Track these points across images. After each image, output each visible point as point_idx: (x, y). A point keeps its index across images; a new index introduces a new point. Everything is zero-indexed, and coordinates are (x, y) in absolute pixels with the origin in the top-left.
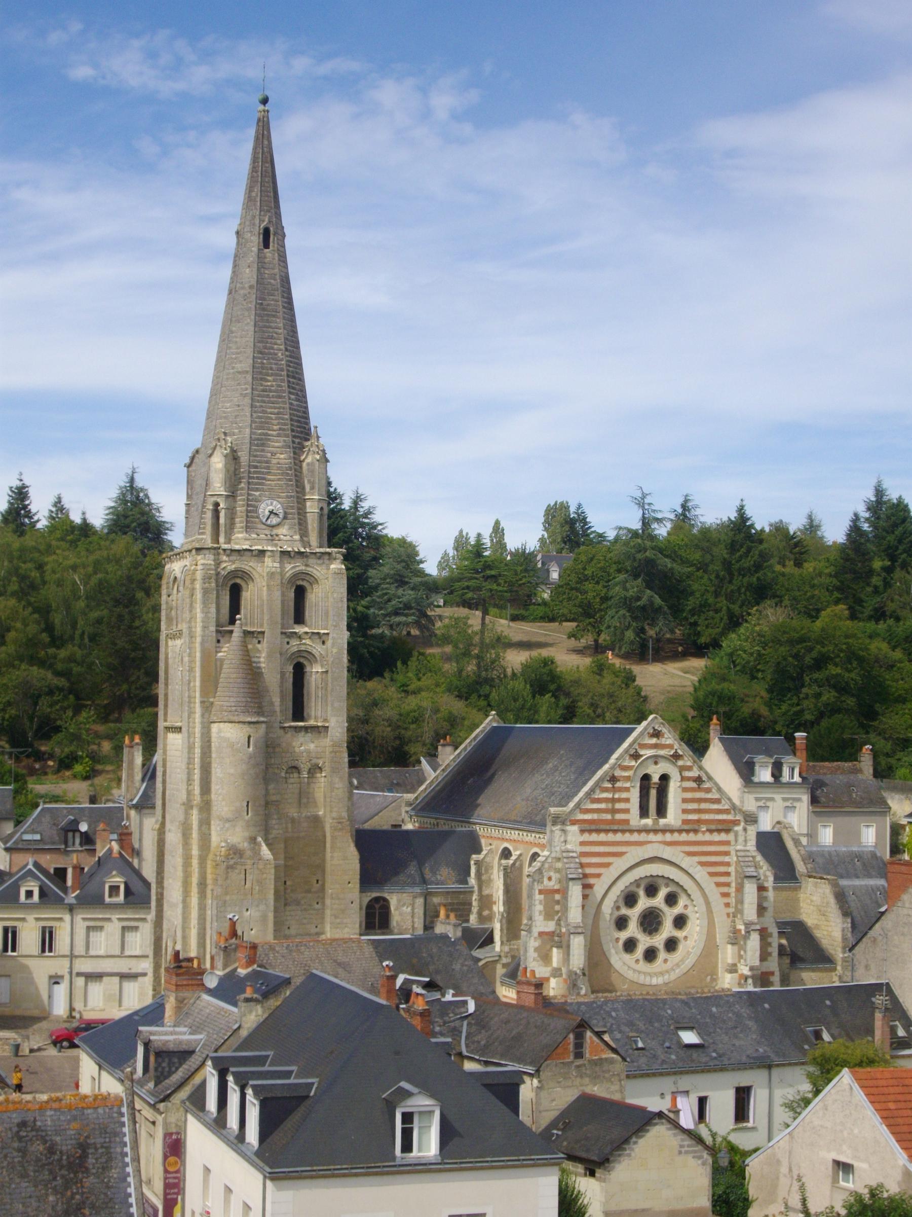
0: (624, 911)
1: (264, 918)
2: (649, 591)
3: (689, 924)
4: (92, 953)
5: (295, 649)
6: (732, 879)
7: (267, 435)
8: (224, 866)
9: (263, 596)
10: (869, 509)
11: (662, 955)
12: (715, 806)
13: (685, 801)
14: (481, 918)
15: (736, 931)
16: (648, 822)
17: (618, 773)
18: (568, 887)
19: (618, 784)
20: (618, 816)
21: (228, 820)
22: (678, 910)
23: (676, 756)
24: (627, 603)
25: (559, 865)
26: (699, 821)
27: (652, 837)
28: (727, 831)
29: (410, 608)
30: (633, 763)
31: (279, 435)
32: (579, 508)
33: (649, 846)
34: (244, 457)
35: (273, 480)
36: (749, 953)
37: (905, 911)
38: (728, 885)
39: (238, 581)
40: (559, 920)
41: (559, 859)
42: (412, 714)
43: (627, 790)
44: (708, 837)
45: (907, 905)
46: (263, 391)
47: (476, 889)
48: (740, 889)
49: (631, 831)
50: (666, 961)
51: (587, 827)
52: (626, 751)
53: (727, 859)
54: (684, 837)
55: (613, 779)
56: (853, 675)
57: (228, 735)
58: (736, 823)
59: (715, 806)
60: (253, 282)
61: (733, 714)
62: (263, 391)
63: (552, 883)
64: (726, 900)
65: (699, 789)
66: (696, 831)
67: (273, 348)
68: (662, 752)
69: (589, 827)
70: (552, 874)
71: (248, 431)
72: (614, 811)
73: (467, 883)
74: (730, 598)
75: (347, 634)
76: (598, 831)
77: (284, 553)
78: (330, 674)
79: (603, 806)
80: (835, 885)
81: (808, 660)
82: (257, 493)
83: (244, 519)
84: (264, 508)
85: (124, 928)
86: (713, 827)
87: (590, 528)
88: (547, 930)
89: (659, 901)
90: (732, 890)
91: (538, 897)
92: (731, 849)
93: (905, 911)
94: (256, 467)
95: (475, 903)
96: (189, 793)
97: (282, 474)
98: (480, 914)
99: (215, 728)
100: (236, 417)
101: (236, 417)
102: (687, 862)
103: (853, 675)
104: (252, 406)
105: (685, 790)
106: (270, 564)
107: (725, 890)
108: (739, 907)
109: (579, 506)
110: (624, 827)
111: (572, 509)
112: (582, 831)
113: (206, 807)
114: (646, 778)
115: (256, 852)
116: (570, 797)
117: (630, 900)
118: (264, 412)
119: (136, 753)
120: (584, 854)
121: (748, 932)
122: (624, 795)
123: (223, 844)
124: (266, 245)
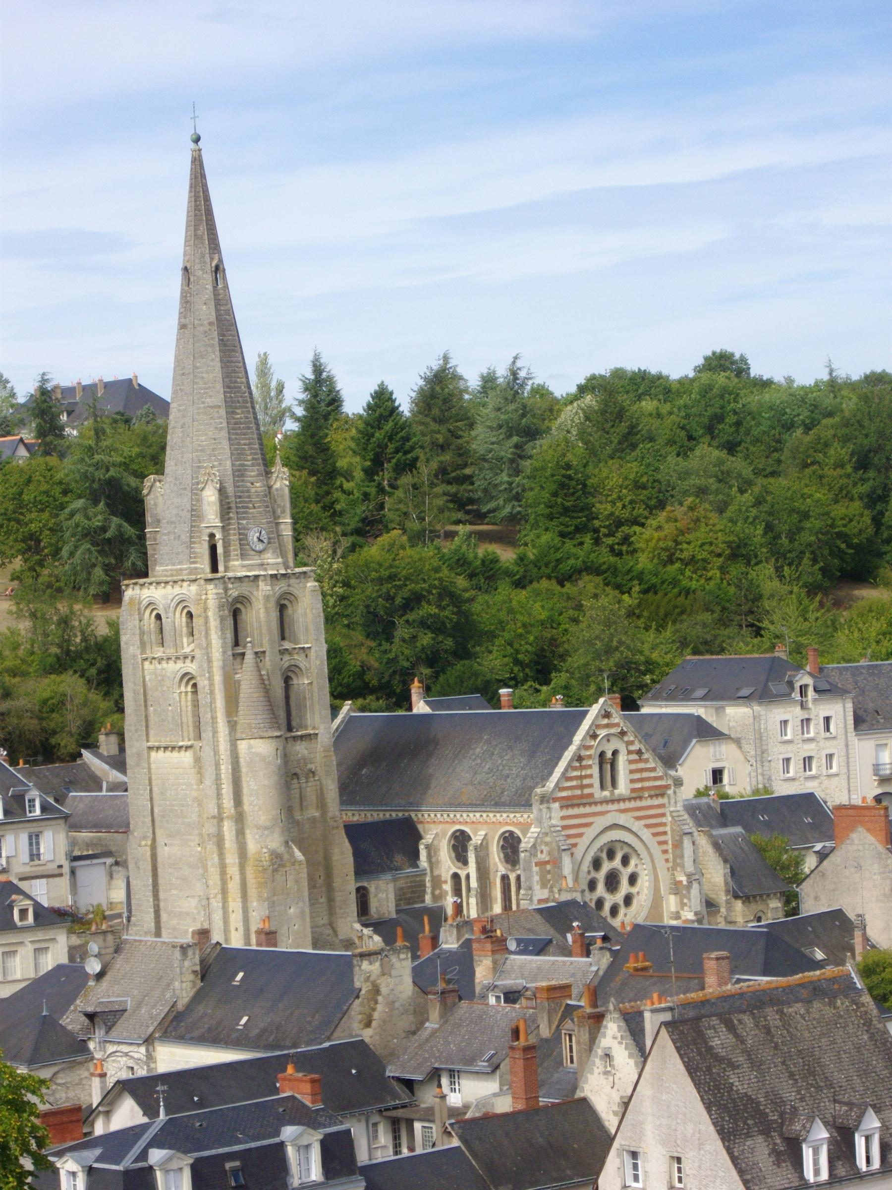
0: (593, 874)
1: (303, 912)
2: (115, 518)
3: (639, 881)
4: (10, 978)
5: (287, 665)
6: (668, 837)
8: (270, 871)
9: (259, 616)
10: (306, 389)
11: (622, 910)
12: (652, 774)
13: (631, 772)
14: (435, 898)
15: (678, 883)
16: (606, 793)
17: (584, 753)
18: (561, 858)
19: (584, 763)
20: (587, 791)
21: (266, 828)
22: (631, 869)
23: (623, 733)
24: (93, 535)
25: (548, 839)
26: (642, 789)
27: (611, 807)
28: (662, 795)
30: (592, 743)
31: (253, 465)
33: (609, 815)
34: (230, 490)
36: (693, 900)
37: (855, 847)
38: (665, 842)
39: (239, 606)
40: (551, 887)
41: (546, 834)
42: (50, 702)
43: (590, 767)
44: (649, 802)
45: (856, 842)
47: (428, 871)
48: (678, 845)
49: (596, 803)
50: (625, 915)
51: (565, 803)
52: (587, 732)
53: (664, 820)
54: (633, 804)
55: (580, 758)
56: (447, 613)
57: (259, 750)
58: (667, 787)
59: (652, 774)
60: (213, 318)
61: (342, 668)
63: (544, 856)
64: (665, 856)
65: (640, 760)
66: (641, 798)
67: (236, 382)
69: (568, 803)
70: (543, 847)
71: (229, 463)
72: (582, 787)
73: (417, 866)
76: (573, 806)
79: (574, 783)
80: (711, 836)
81: (398, 601)
82: (244, 522)
84: (253, 536)
85: (36, 950)
86: (652, 793)
88: (543, 897)
89: (617, 862)
90: (669, 847)
91: (535, 869)
92: (666, 810)
93: (855, 847)
94: (240, 497)
95: (428, 884)
96: (220, 807)
98: (433, 893)
99: (242, 746)
100: (213, 450)
101: (213, 450)
102: (637, 826)
103: (447, 613)
104: (230, 439)
105: (631, 762)
106: (264, 588)
107: (664, 847)
108: (678, 861)
110: (587, 800)
112: (562, 807)
113: (240, 818)
114: (602, 755)
115: (292, 855)
117: (597, 864)
118: (239, 444)
120: (565, 828)
121: (690, 883)
122: (589, 772)
123: (265, 850)
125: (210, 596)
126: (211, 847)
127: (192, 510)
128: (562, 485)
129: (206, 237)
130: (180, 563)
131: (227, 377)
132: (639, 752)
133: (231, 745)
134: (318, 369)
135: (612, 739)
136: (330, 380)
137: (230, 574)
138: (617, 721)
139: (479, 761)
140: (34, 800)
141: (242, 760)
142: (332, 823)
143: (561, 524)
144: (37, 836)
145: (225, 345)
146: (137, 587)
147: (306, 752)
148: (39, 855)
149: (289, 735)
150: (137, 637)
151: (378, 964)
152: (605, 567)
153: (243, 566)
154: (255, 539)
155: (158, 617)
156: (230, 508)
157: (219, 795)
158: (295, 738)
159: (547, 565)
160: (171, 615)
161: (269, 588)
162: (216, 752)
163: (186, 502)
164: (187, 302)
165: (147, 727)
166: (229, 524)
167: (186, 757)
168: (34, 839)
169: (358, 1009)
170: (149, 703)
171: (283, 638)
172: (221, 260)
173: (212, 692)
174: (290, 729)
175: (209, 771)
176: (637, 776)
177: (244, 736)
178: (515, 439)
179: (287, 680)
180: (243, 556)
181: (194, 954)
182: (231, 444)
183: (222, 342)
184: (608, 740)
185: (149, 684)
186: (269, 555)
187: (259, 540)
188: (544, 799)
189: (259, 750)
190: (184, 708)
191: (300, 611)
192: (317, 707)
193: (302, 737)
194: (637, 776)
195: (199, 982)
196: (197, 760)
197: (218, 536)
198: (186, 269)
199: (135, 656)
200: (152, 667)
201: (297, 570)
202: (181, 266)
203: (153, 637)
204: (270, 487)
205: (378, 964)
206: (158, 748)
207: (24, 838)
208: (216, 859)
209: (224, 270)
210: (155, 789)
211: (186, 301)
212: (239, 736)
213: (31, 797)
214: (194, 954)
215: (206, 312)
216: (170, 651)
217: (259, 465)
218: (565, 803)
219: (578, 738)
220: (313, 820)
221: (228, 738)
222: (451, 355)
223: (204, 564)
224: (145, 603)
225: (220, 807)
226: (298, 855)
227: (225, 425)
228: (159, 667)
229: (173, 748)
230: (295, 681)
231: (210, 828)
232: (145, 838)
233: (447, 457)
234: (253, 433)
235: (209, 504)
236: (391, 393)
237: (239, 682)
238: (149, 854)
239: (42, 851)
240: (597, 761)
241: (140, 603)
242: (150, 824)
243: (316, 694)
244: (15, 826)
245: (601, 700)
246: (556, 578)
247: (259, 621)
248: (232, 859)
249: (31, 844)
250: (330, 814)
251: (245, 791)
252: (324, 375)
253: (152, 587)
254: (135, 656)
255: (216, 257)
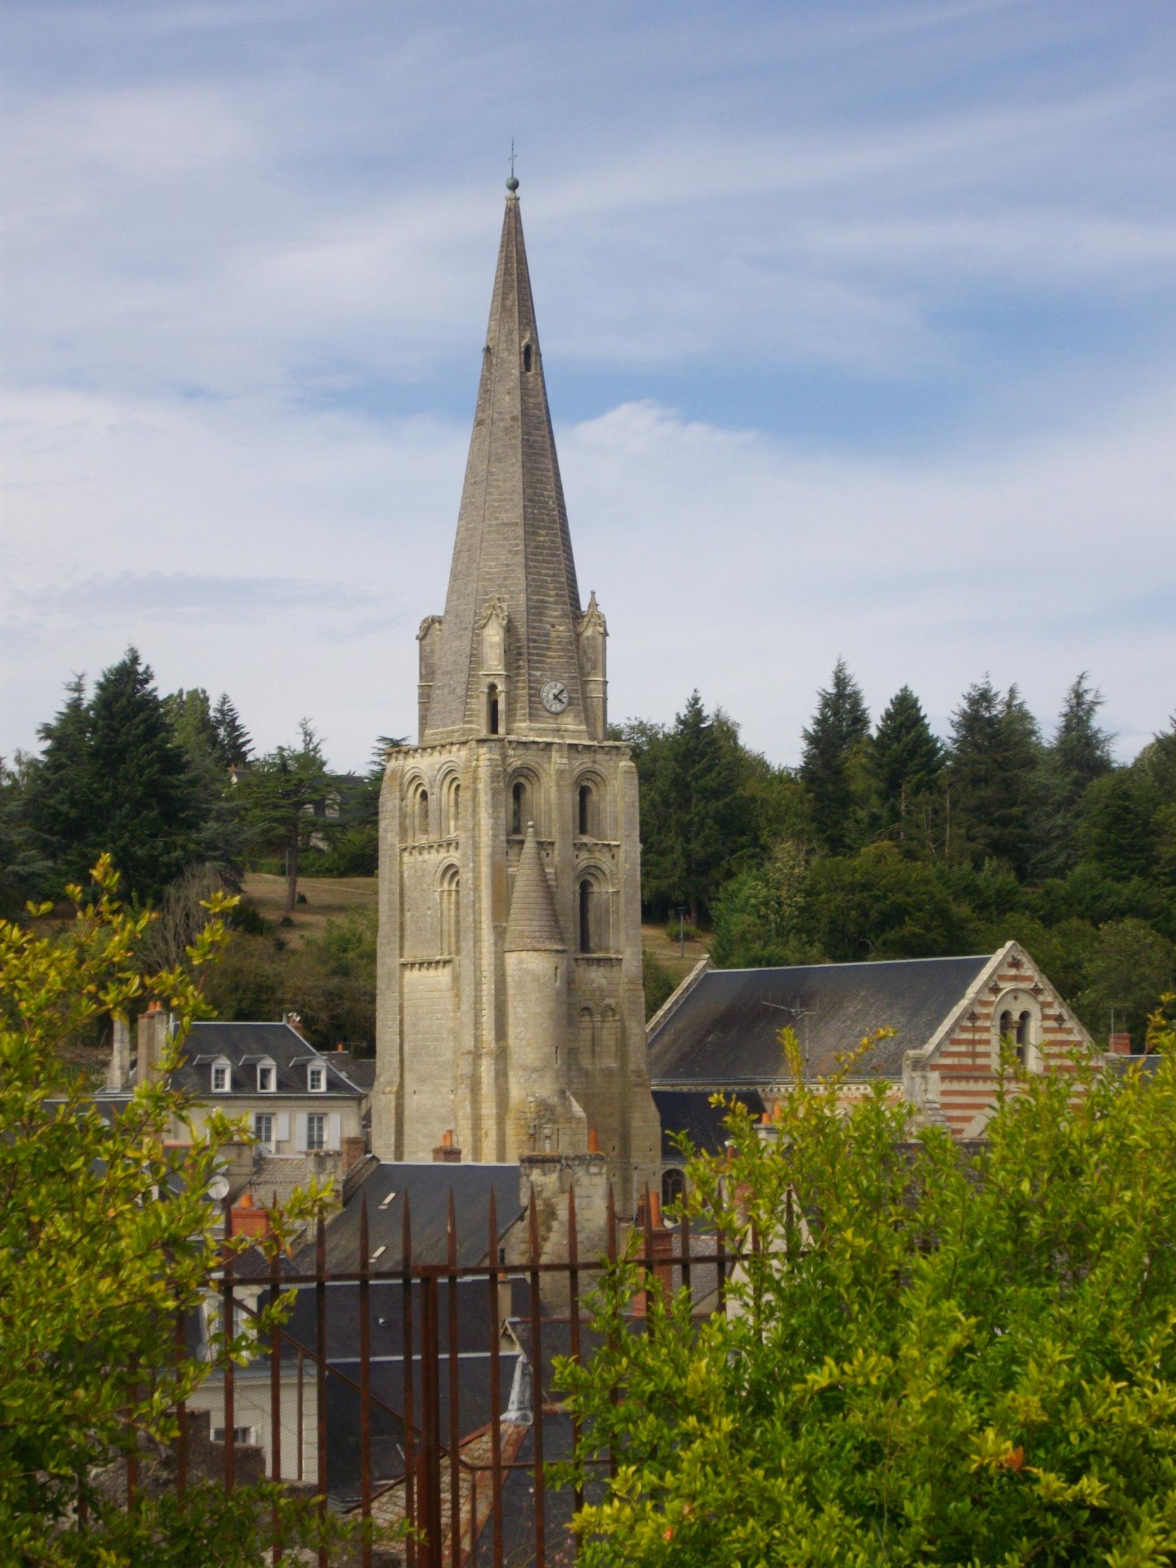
5: (584, 864)
7: (542, 601)
9: (550, 796)
17: (979, 1010)
19: (979, 1023)
20: (980, 1061)
21: (535, 1070)
23: (1036, 991)
29: (216, 848)
30: (992, 998)
31: (556, 603)
32: (224, 703)
34: (522, 630)
35: (554, 658)
39: (522, 780)
43: (987, 1029)
46: (537, 547)
52: (986, 983)
55: (973, 1017)
57: (533, 966)
60: (517, 411)
62: (537, 547)
65: (1060, 1030)
68: (1022, 985)
69: (951, 1074)
71: (523, 597)
72: (974, 1055)
74: (684, 831)
75: (639, 847)
76: (959, 1078)
77: (571, 747)
78: (622, 895)
79: (963, 1048)
81: (874, 915)
83: (526, 705)
84: (549, 691)
87: (241, 735)
96: (477, 1038)
97: (563, 650)
99: (511, 959)
100: (505, 579)
101: (505, 579)
103: (933, 935)
104: (526, 566)
105: (1046, 1030)
106: (558, 759)
109: (225, 700)
111: (214, 703)
112: (943, 1079)
113: (502, 1055)
114: (1005, 1016)
115: (568, 1109)
116: (924, 1042)
119: (158, 1026)
120: (945, 1106)
122: (985, 1036)
123: (531, 1099)
124: (528, 369)
125: (482, 763)
126: (464, 1091)
127: (472, 655)
128: (1117, 819)
129: (516, 309)
130: (453, 723)
131: (530, 487)
132: (1059, 1018)
133: (497, 958)
134: (841, 681)
135: (1023, 997)
136: (855, 698)
137: (512, 737)
138: (1029, 973)
139: (849, 1022)
140: (319, 1073)
141: (509, 980)
142: (633, 1078)
143: (1113, 866)
144: (321, 1120)
145: (531, 447)
146: (401, 756)
147: (604, 982)
148: (320, 1143)
149: (580, 956)
150: (397, 821)
151: (554, 1176)
152: (1155, 910)
153: (531, 729)
154: (551, 697)
155: (424, 795)
156: (520, 654)
157: (477, 1024)
158: (589, 961)
159: (1080, 902)
160: (436, 790)
161: (565, 761)
162: (477, 967)
163: (465, 644)
164: (487, 391)
165: (402, 938)
166: (518, 675)
167: (443, 976)
168: (316, 1122)
169: (521, 1235)
170: (406, 907)
171: (583, 830)
172: (535, 339)
173: (476, 889)
174: (584, 946)
175: (468, 991)
176: (1055, 1050)
177: (513, 947)
178: (1075, 773)
179: (585, 887)
180: (532, 716)
181: (335, 1167)
182: (528, 573)
183: (527, 444)
184: (1016, 998)
185: (407, 882)
186: (569, 720)
187: (556, 697)
188: (918, 1064)
189: (532, 967)
190: (445, 912)
191: (609, 798)
192: (623, 926)
193: (599, 961)
194: (1055, 1050)
195: (340, 1205)
196: (456, 978)
197: (500, 687)
198: (488, 350)
199: (392, 846)
200: (412, 859)
201: (607, 743)
202: (484, 345)
203: (417, 822)
204: (579, 635)
205: (554, 1176)
206: (413, 965)
207: (302, 1119)
208: (468, 1109)
209: (539, 355)
210: (407, 1019)
211: (486, 391)
212: (507, 946)
213: (316, 1069)
214: (335, 1167)
215: (509, 403)
216: (433, 837)
217: (565, 603)
218: (947, 1073)
219: (971, 991)
220: (609, 1072)
221: (492, 949)
222: (1019, 689)
223: (481, 727)
224: (408, 776)
225: (477, 1038)
226: (577, 1109)
227: (521, 547)
228: (420, 858)
229: (430, 964)
230: (595, 888)
231: (465, 1068)
232: (390, 1083)
233: (987, 792)
234: (559, 562)
235: (491, 645)
236: (916, 700)
237: (513, 877)
238: (393, 1103)
239: (325, 1138)
240: (998, 1022)
241: (402, 777)
242: (397, 1065)
243: (622, 907)
244: (292, 1103)
245: (1009, 944)
246: (1091, 918)
247: (548, 803)
248: (489, 1109)
249: (310, 1129)
250: (632, 1066)
251: (511, 1020)
252: (849, 690)
253: (418, 755)
254: (392, 846)
255: (528, 335)
